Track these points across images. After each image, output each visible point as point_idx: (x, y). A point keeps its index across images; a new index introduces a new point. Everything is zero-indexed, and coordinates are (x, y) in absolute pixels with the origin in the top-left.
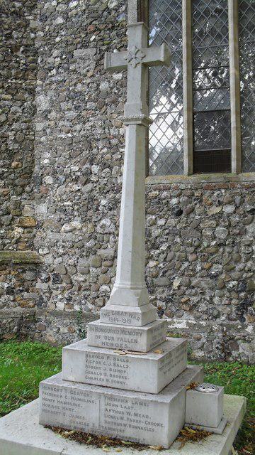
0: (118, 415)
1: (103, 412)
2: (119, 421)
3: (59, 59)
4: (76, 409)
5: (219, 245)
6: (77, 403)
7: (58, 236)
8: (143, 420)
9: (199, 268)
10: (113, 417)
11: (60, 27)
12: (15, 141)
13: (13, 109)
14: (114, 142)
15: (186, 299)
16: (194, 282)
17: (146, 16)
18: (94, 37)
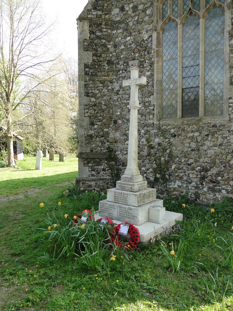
0: (123, 213)
1: (119, 212)
2: (124, 215)
3: (123, 66)
4: (110, 211)
5: (192, 150)
6: (111, 209)
7: (123, 146)
8: (131, 215)
9: (183, 161)
10: (121, 214)
11: (122, 50)
12: (105, 105)
13: (103, 91)
14: (147, 104)
15: (178, 174)
16: (181, 166)
17: (161, 42)
18: (137, 55)
